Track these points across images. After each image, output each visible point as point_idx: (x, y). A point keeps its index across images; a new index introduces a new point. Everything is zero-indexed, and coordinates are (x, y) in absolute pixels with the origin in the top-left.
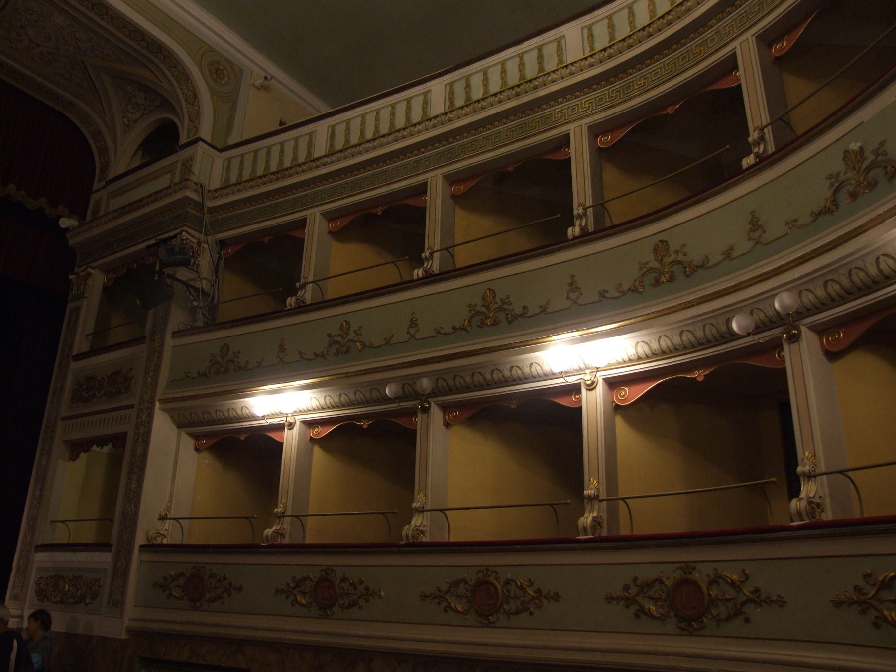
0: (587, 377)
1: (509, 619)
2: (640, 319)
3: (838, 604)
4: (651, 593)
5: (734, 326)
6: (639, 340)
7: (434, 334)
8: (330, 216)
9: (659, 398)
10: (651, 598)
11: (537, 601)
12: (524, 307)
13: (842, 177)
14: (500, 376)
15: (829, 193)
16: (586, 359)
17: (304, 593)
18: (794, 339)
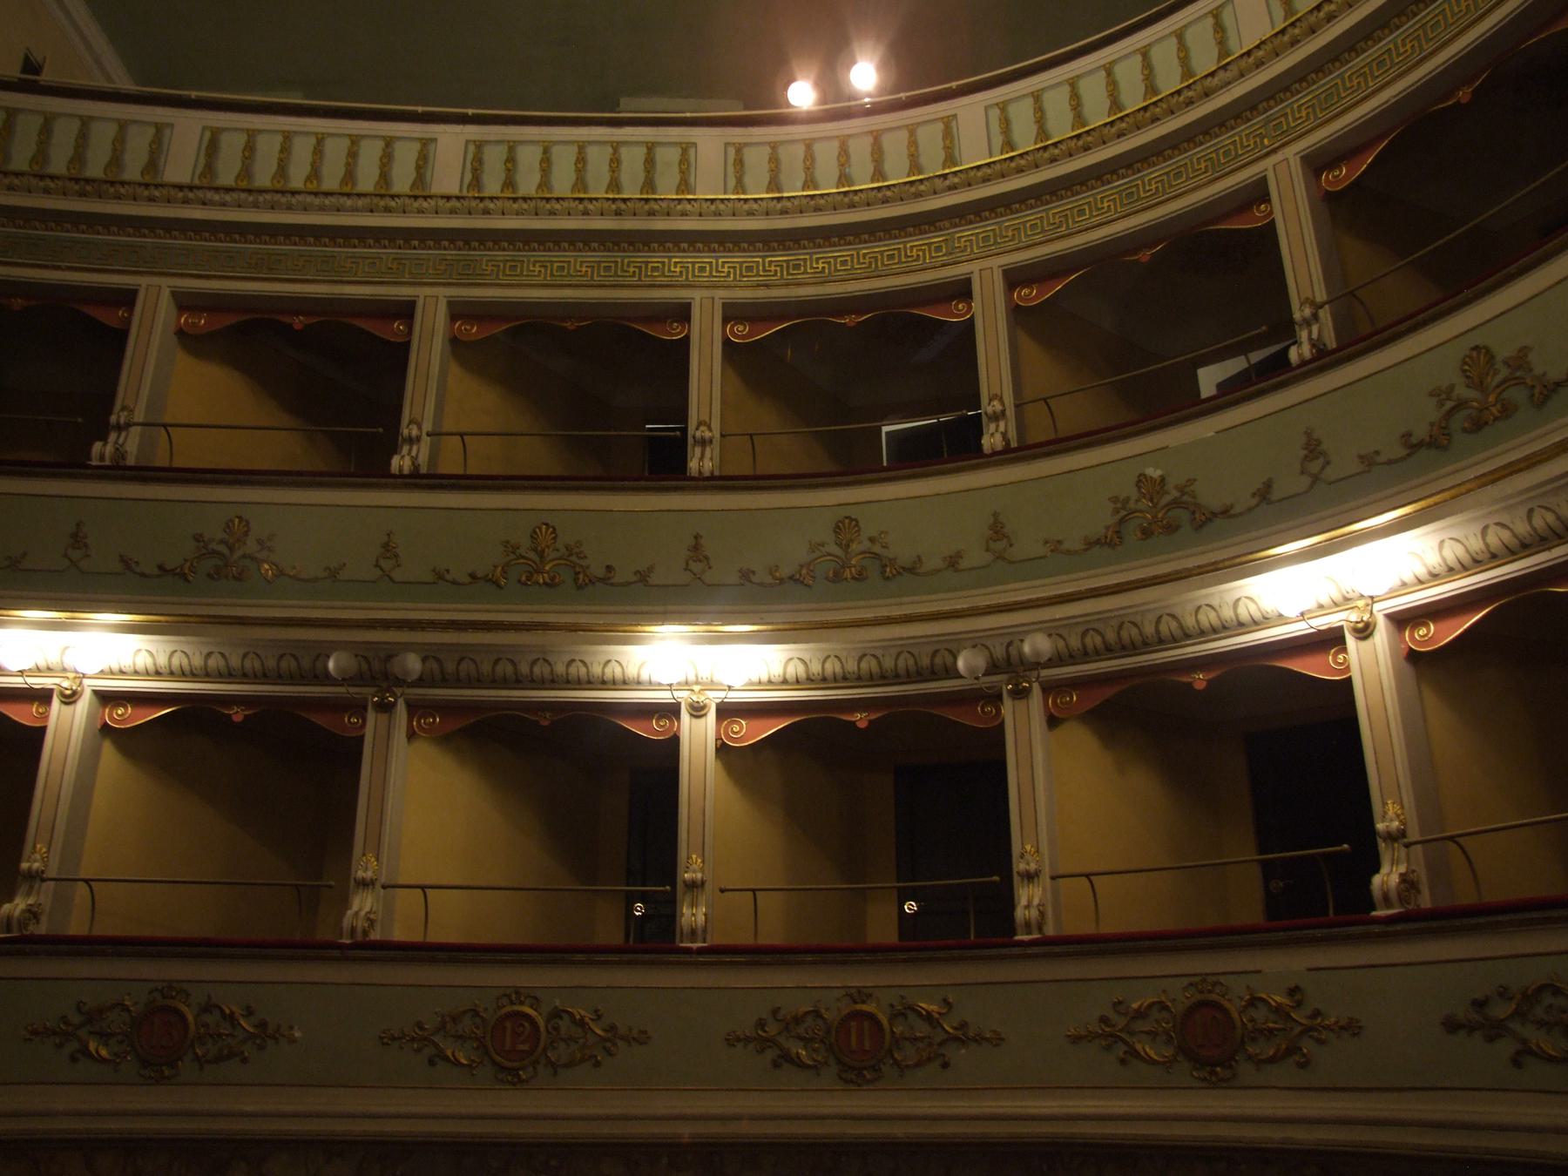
0: (66, 684)
1: (201, 1068)
3: (1076, 1040)
4: (801, 1030)
7: (430, 577)
8: (458, 312)
9: (797, 750)
10: (801, 1038)
11: (608, 1045)
12: (609, 568)
13: (1132, 505)
14: (547, 670)
15: (1112, 520)
16: (699, 669)
17: (104, 1036)
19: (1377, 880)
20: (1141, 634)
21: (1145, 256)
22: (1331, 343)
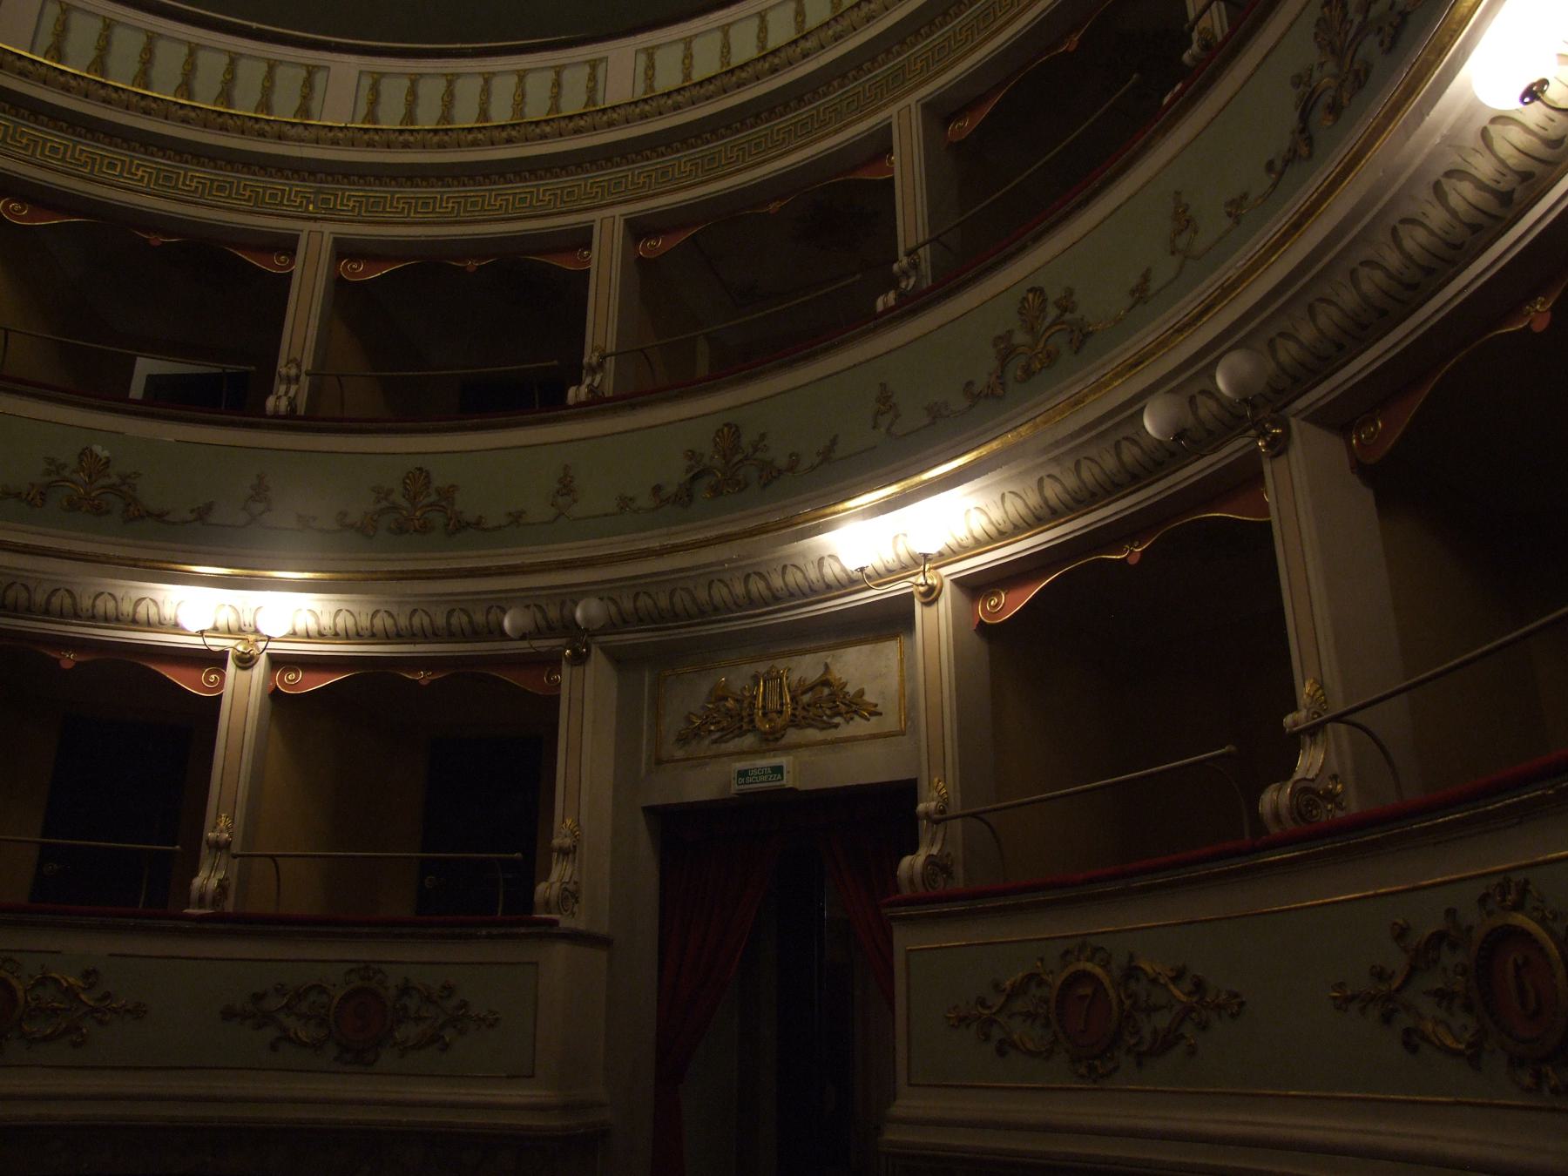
2: (346, 576)
5: (507, 623)
6: (344, 606)
9: (327, 707)
13: (66, 473)
18: (579, 659)
19: (197, 882)
20: (29, 599)
21: (157, 240)
22: (301, 411)
